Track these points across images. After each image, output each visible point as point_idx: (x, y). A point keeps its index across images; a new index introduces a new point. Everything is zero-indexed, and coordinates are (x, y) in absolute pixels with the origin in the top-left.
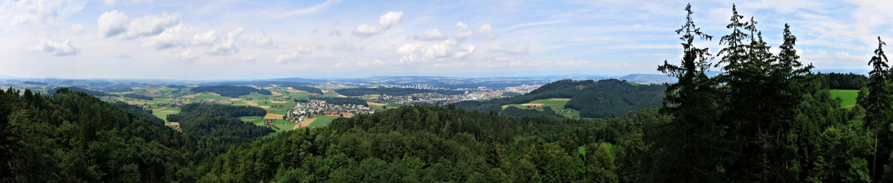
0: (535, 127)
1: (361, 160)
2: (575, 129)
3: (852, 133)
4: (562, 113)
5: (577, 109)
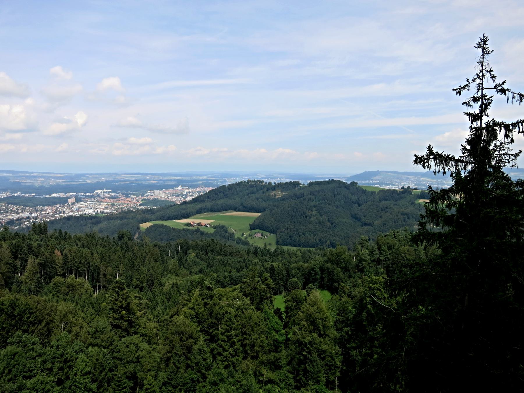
0: (199, 260)
2: (268, 266)
4: (246, 238)
5: (272, 232)
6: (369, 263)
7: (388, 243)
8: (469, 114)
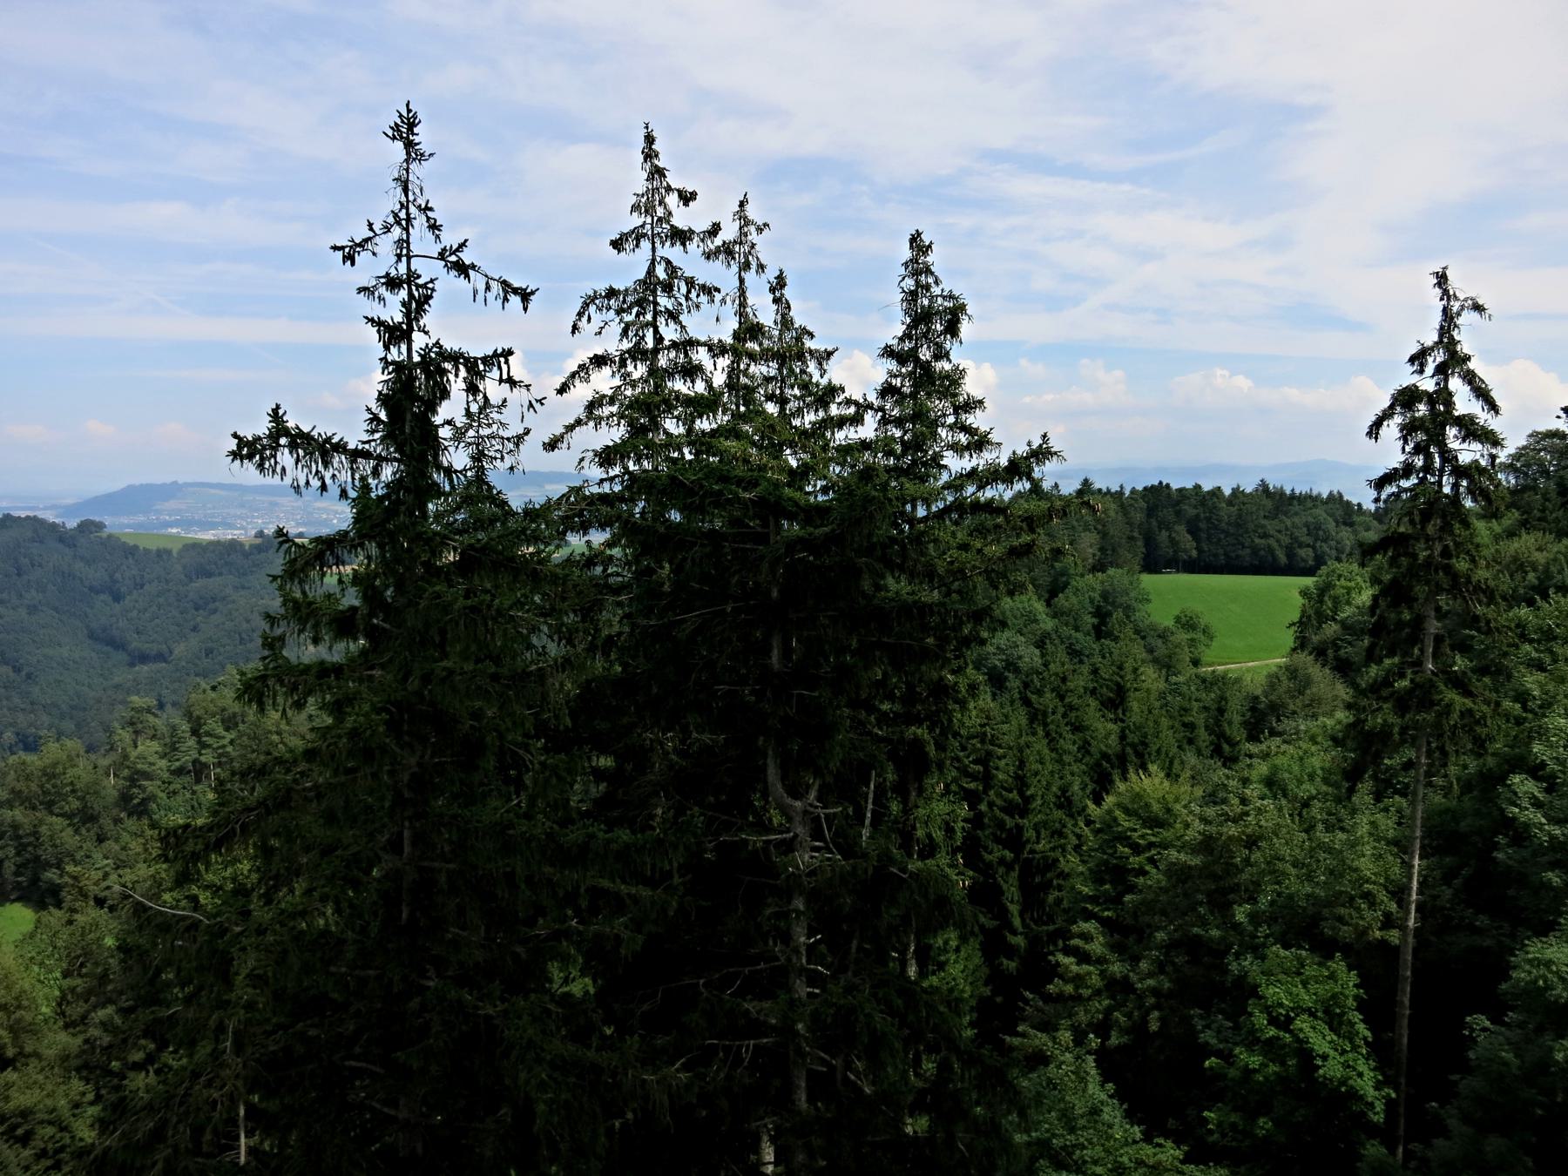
3: (1269, 813)
6: (164, 782)
7: (224, 710)
8: (378, 323)
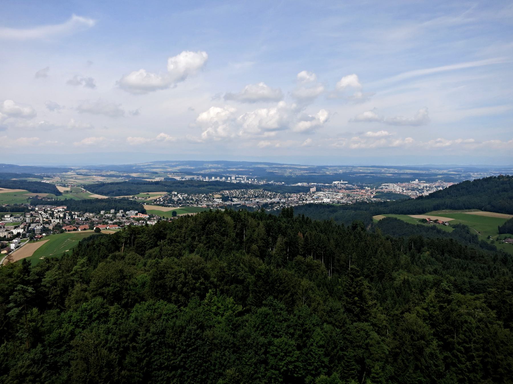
1: (132, 306)
4: (493, 242)
